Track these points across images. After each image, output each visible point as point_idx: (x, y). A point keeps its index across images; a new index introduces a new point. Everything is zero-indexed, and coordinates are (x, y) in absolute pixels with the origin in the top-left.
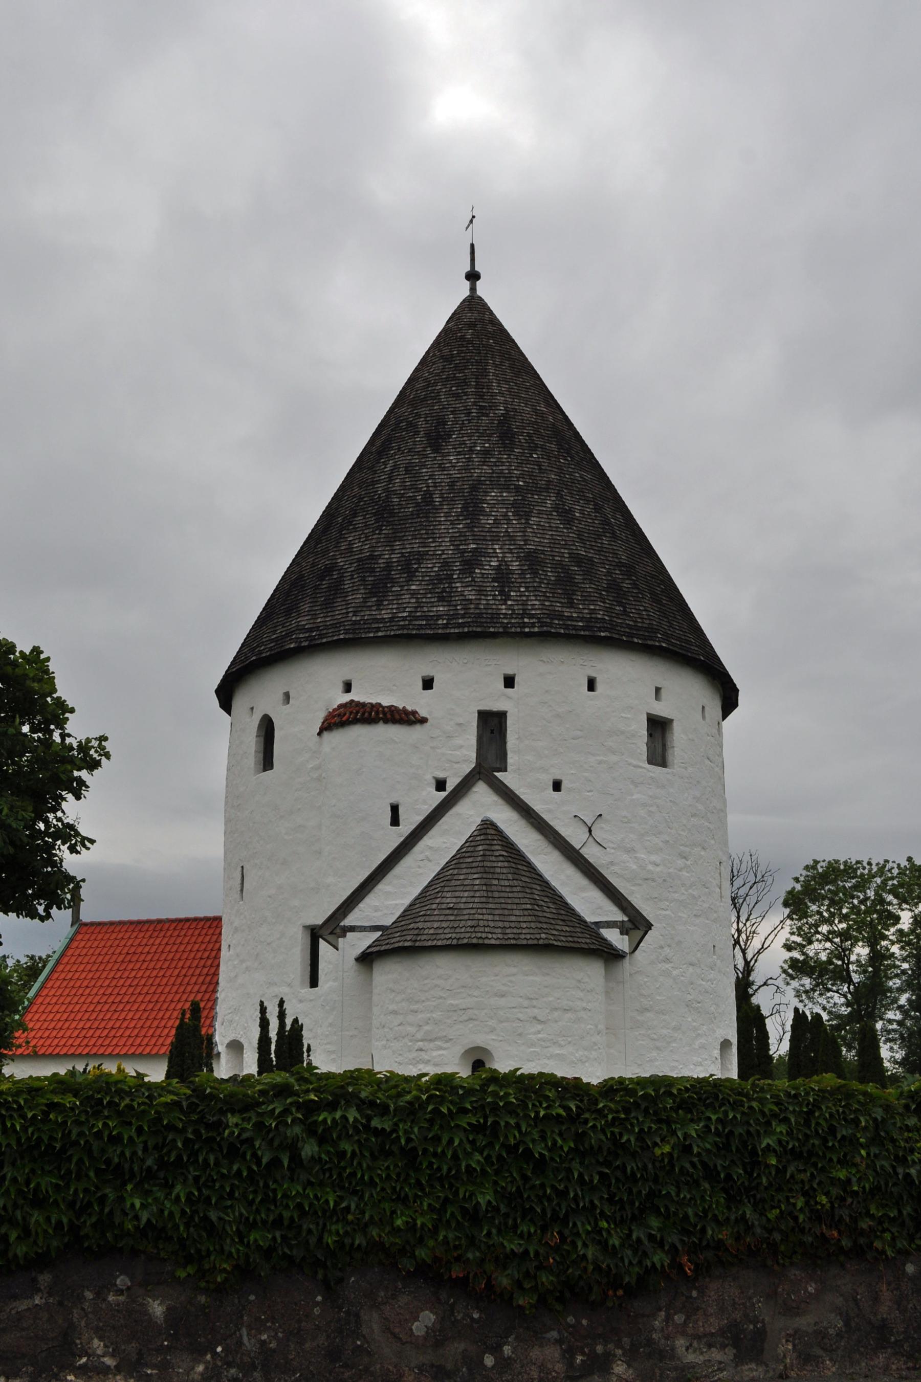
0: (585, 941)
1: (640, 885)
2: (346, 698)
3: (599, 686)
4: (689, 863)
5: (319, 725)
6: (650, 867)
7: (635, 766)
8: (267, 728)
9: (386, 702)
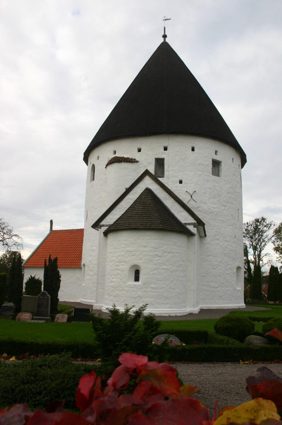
1: (208, 214)
3: (195, 149)
4: (226, 208)
6: (212, 209)
7: (207, 176)
8: (93, 167)
9: (126, 156)
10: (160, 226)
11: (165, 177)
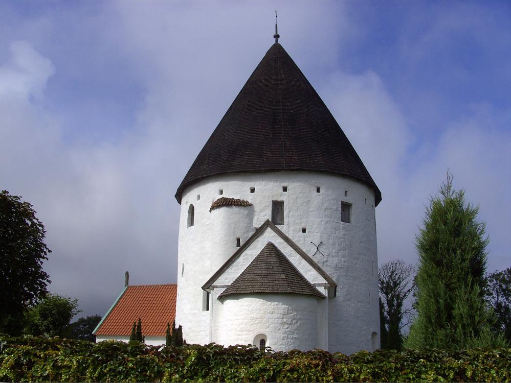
0: (307, 291)
2: (221, 197)
5: (210, 207)
8: (192, 209)
9: (236, 197)
10: (289, 289)
11: (285, 224)
